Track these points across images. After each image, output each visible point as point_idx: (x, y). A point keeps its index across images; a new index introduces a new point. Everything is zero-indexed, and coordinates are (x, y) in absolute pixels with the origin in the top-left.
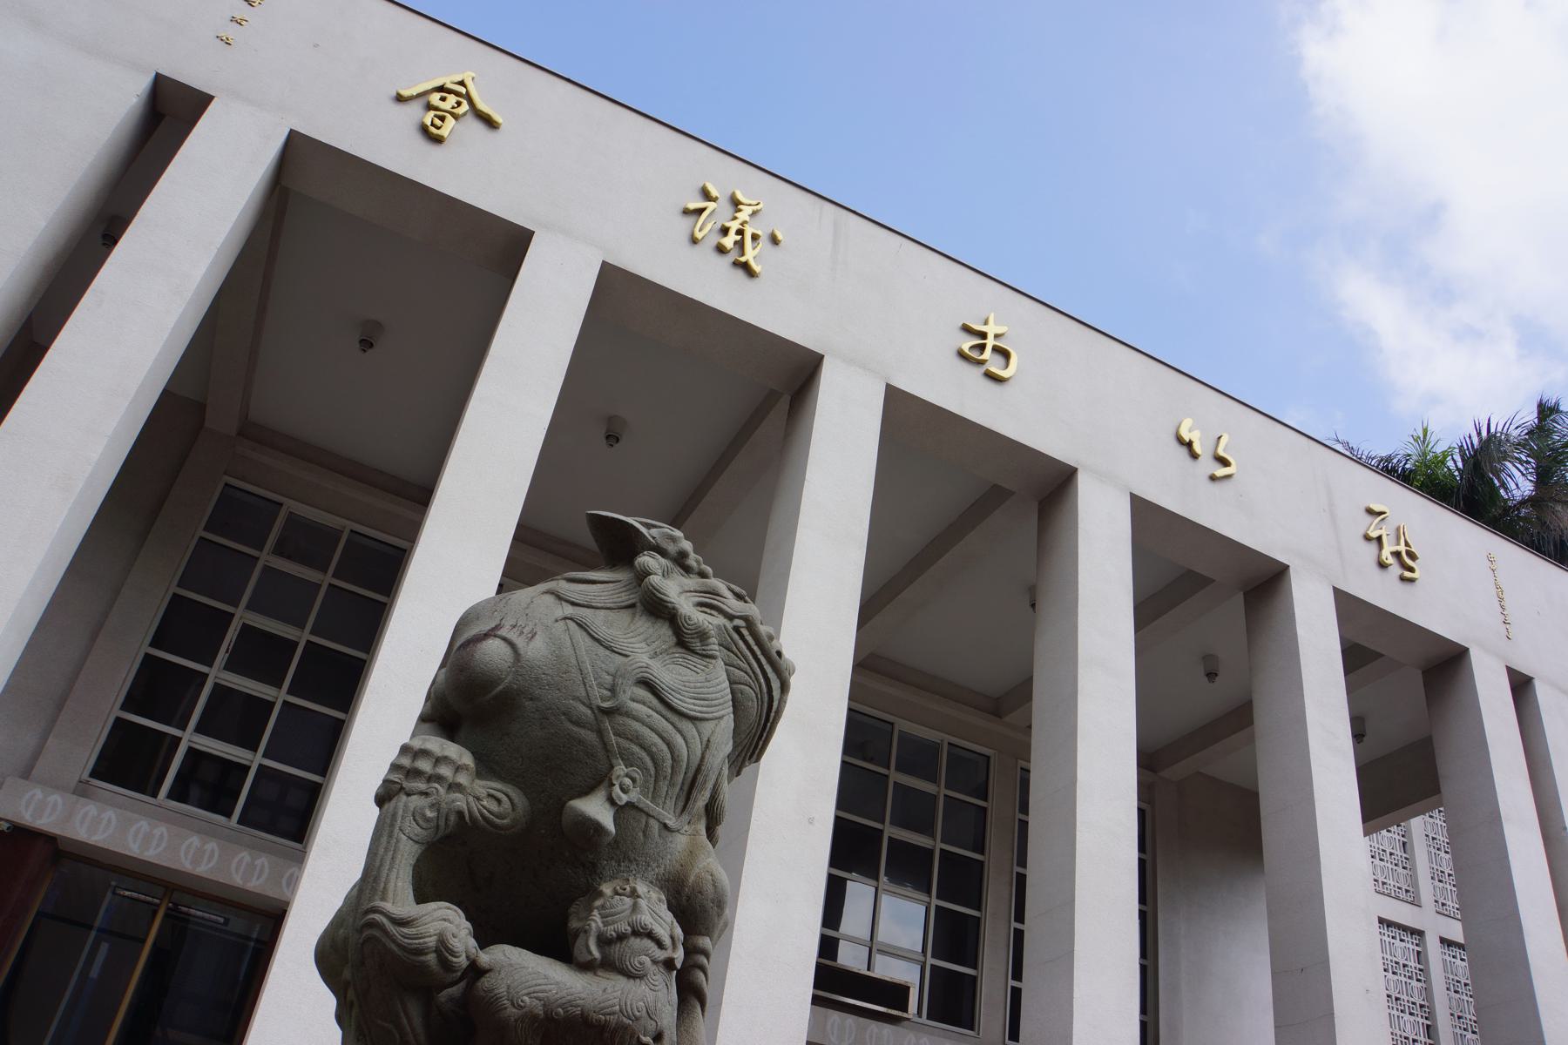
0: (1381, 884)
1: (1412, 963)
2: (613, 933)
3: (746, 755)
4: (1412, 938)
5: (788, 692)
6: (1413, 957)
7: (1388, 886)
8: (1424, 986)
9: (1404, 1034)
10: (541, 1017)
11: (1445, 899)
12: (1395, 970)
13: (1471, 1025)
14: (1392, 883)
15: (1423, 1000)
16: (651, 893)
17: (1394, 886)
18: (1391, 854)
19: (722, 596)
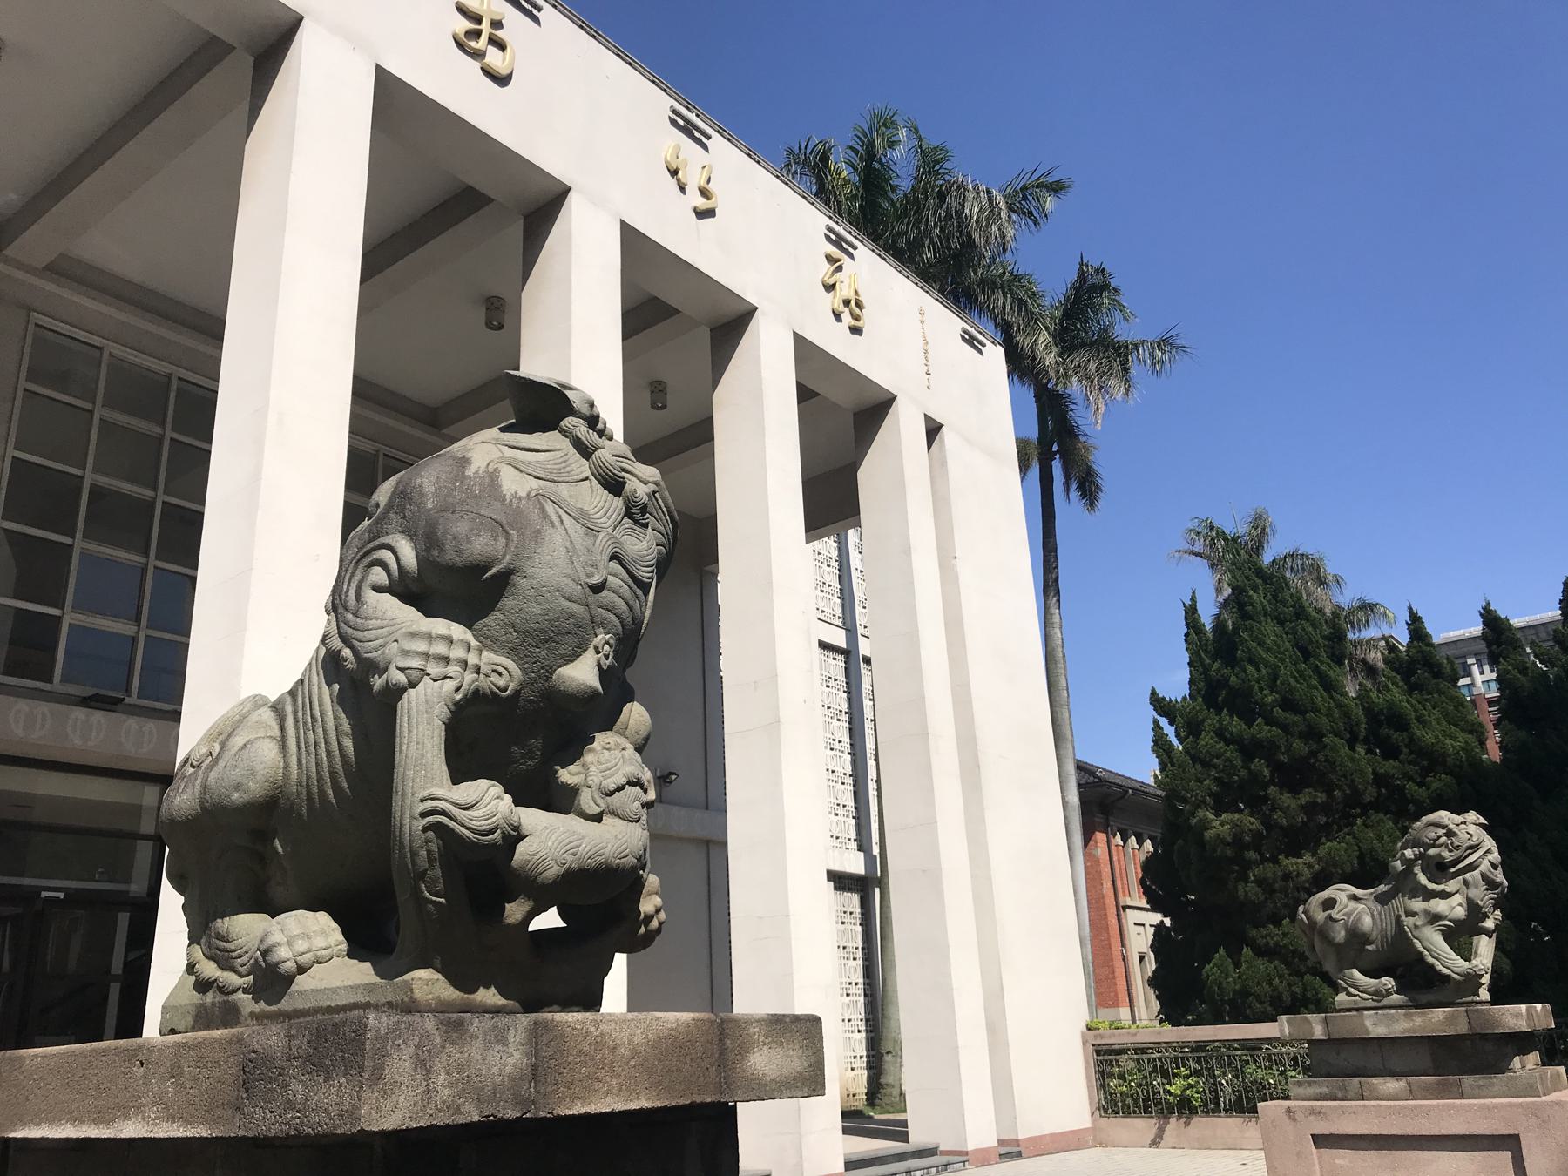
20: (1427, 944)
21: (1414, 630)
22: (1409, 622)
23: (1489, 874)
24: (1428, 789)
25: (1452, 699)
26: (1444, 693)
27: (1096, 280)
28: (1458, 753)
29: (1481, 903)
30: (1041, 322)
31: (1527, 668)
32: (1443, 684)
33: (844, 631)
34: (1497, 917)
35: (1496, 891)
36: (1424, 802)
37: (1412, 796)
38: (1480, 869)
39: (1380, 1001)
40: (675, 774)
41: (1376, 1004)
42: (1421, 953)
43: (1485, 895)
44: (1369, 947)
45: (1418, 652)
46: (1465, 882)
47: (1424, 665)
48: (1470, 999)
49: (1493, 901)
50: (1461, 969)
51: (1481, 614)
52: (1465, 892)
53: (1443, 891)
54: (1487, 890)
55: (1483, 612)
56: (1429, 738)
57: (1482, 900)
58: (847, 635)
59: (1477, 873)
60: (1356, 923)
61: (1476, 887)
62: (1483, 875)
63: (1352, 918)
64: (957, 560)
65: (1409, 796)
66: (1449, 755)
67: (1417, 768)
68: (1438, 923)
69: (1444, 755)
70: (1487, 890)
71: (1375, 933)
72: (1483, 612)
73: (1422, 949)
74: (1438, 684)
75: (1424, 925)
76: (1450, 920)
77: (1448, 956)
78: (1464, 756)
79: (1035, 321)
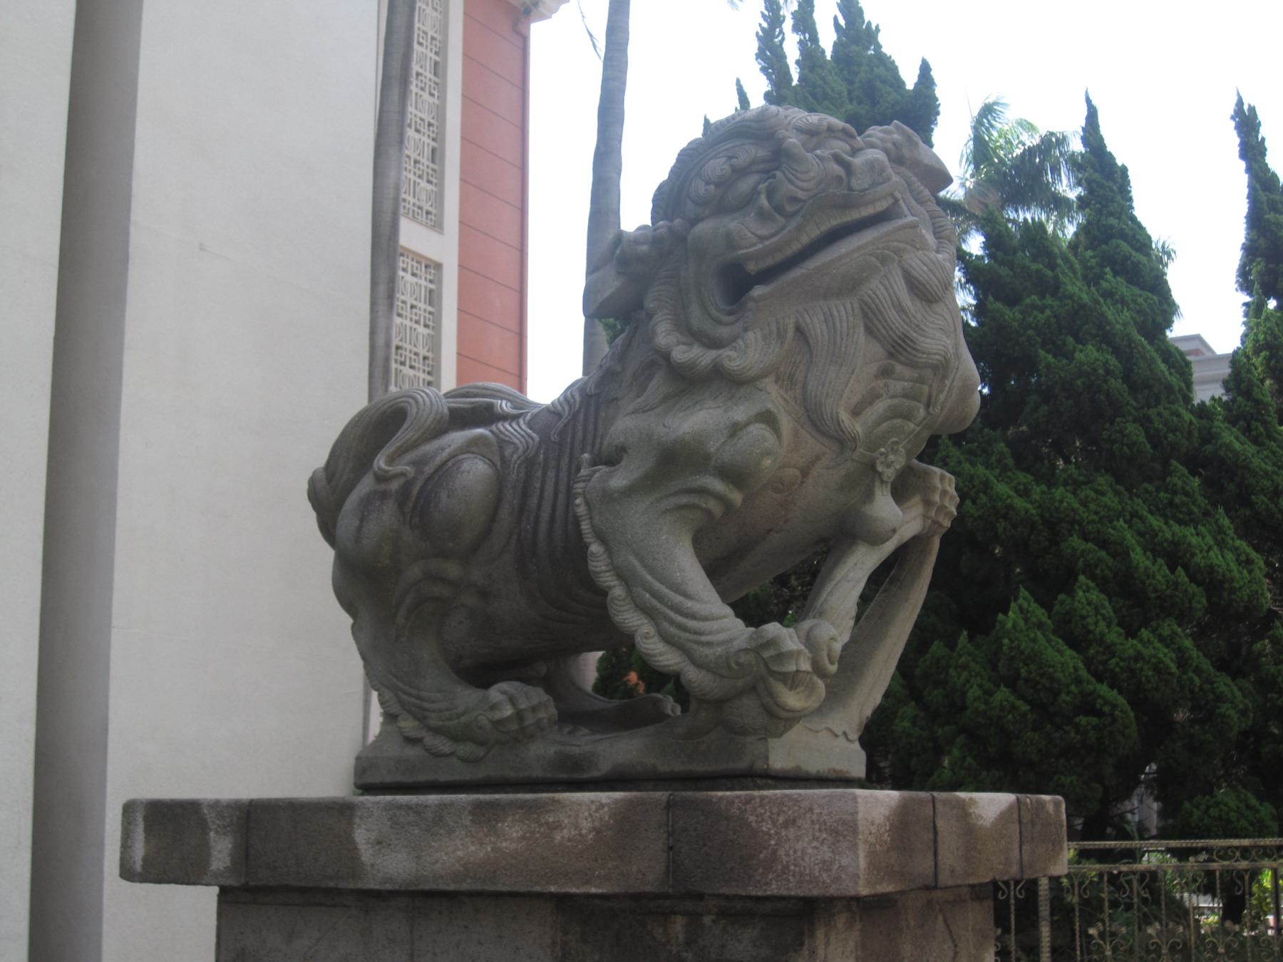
0: (409, 270)
1: (425, 161)
2: (1107, 572)
3: (910, 346)
4: (429, 130)
5: (760, 55)
6: (427, 151)
7: (421, 166)
8: (439, 17)
9: (415, 350)
10: (1207, 391)
11: (401, 340)
12: (415, 271)
13: (410, 358)
14: (431, 33)
15: (433, 118)
16: (802, 806)
17: (414, 205)
18: (416, 162)
19: (499, 499)
73: (608, 579)
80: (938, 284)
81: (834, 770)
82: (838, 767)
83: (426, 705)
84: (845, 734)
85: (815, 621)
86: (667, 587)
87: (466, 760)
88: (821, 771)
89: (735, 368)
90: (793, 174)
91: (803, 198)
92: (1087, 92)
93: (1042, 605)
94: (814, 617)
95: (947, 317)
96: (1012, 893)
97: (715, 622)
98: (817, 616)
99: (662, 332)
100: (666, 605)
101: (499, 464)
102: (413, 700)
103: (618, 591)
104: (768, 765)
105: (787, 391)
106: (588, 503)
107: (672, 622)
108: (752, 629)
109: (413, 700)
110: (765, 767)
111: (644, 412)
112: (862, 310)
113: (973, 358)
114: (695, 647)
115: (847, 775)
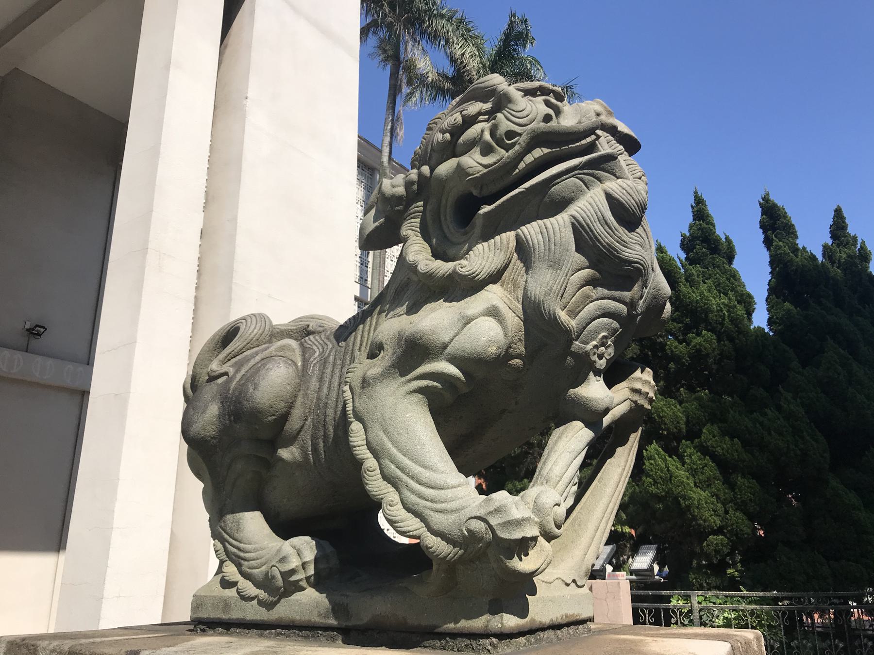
20: (378, 435)
21: (698, 211)
22: (694, 205)
23: (598, 228)
24: (688, 344)
25: (725, 272)
26: (718, 267)
27: (520, 28)
28: (722, 311)
29: (573, 324)
30: (469, 40)
31: (798, 249)
32: (719, 260)
33: (359, 285)
34: (638, 386)
35: (626, 295)
36: (683, 358)
37: (672, 351)
38: (573, 210)
39: (269, 606)
40: (43, 327)
41: (262, 614)
42: (358, 464)
43: (588, 299)
44: (285, 453)
45: (699, 229)
46: (523, 250)
47: (702, 242)
48: (478, 623)
49: (615, 324)
50: (452, 517)
51: (760, 204)
52: (522, 281)
53: (453, 276)
54: (591, 282)
55: (762, 201)
56: (696, 296)
57: (573, 313)
58: (360, 287)
59: (560, 224)
60: (243, 385)
61: (555, 264)
62: (580, 231)
63: (243, 371)
64: (248, 100)
65: (668, 352)
66: (712, 312)
67: (680, 325)
68: (421, 370)
69: (707, 311)
70: (591, 282)
71: (297, 413)
72: (762, 201)
73: (363, 452)
74: (714, 259)
75: (383, 376)
76: (453, 360)
77: (426, 475)
78: (726, 314)
79: (466, 41)
80: (635, 205)
81: (566, 616)
82: (570, 612)
83: (242, 554)
84: (574, 581)
85: (541, 488)
86: (409, 459)
87: (261, 603)
88: (555, 619)
89: (466, 273)
90: (509, 113)
91: (520, 132)
92: (696, 193)
93: (193, 392)
94: (542, 484)
95: (643, 236)
96: (679, 620)
97: (449, 490)
98: (544, 482)
99: (412, 252)
100: (407, 474)
101: (300, 364)
102: (235, 550)
103: (371, 462)
104: (502, 624)
105: (510, 293)
106: (351, 389)
107: (412, 491)
108: (485, 497)
109: (235, 550)
110: (500, 626)
111: (399, 316)
112: (573, 224)
113: (665, 278)
114: (432, 513)
115: (578, 617)
